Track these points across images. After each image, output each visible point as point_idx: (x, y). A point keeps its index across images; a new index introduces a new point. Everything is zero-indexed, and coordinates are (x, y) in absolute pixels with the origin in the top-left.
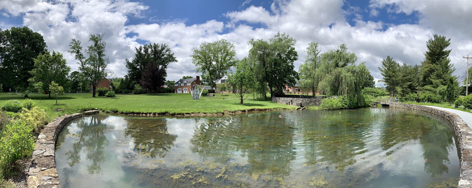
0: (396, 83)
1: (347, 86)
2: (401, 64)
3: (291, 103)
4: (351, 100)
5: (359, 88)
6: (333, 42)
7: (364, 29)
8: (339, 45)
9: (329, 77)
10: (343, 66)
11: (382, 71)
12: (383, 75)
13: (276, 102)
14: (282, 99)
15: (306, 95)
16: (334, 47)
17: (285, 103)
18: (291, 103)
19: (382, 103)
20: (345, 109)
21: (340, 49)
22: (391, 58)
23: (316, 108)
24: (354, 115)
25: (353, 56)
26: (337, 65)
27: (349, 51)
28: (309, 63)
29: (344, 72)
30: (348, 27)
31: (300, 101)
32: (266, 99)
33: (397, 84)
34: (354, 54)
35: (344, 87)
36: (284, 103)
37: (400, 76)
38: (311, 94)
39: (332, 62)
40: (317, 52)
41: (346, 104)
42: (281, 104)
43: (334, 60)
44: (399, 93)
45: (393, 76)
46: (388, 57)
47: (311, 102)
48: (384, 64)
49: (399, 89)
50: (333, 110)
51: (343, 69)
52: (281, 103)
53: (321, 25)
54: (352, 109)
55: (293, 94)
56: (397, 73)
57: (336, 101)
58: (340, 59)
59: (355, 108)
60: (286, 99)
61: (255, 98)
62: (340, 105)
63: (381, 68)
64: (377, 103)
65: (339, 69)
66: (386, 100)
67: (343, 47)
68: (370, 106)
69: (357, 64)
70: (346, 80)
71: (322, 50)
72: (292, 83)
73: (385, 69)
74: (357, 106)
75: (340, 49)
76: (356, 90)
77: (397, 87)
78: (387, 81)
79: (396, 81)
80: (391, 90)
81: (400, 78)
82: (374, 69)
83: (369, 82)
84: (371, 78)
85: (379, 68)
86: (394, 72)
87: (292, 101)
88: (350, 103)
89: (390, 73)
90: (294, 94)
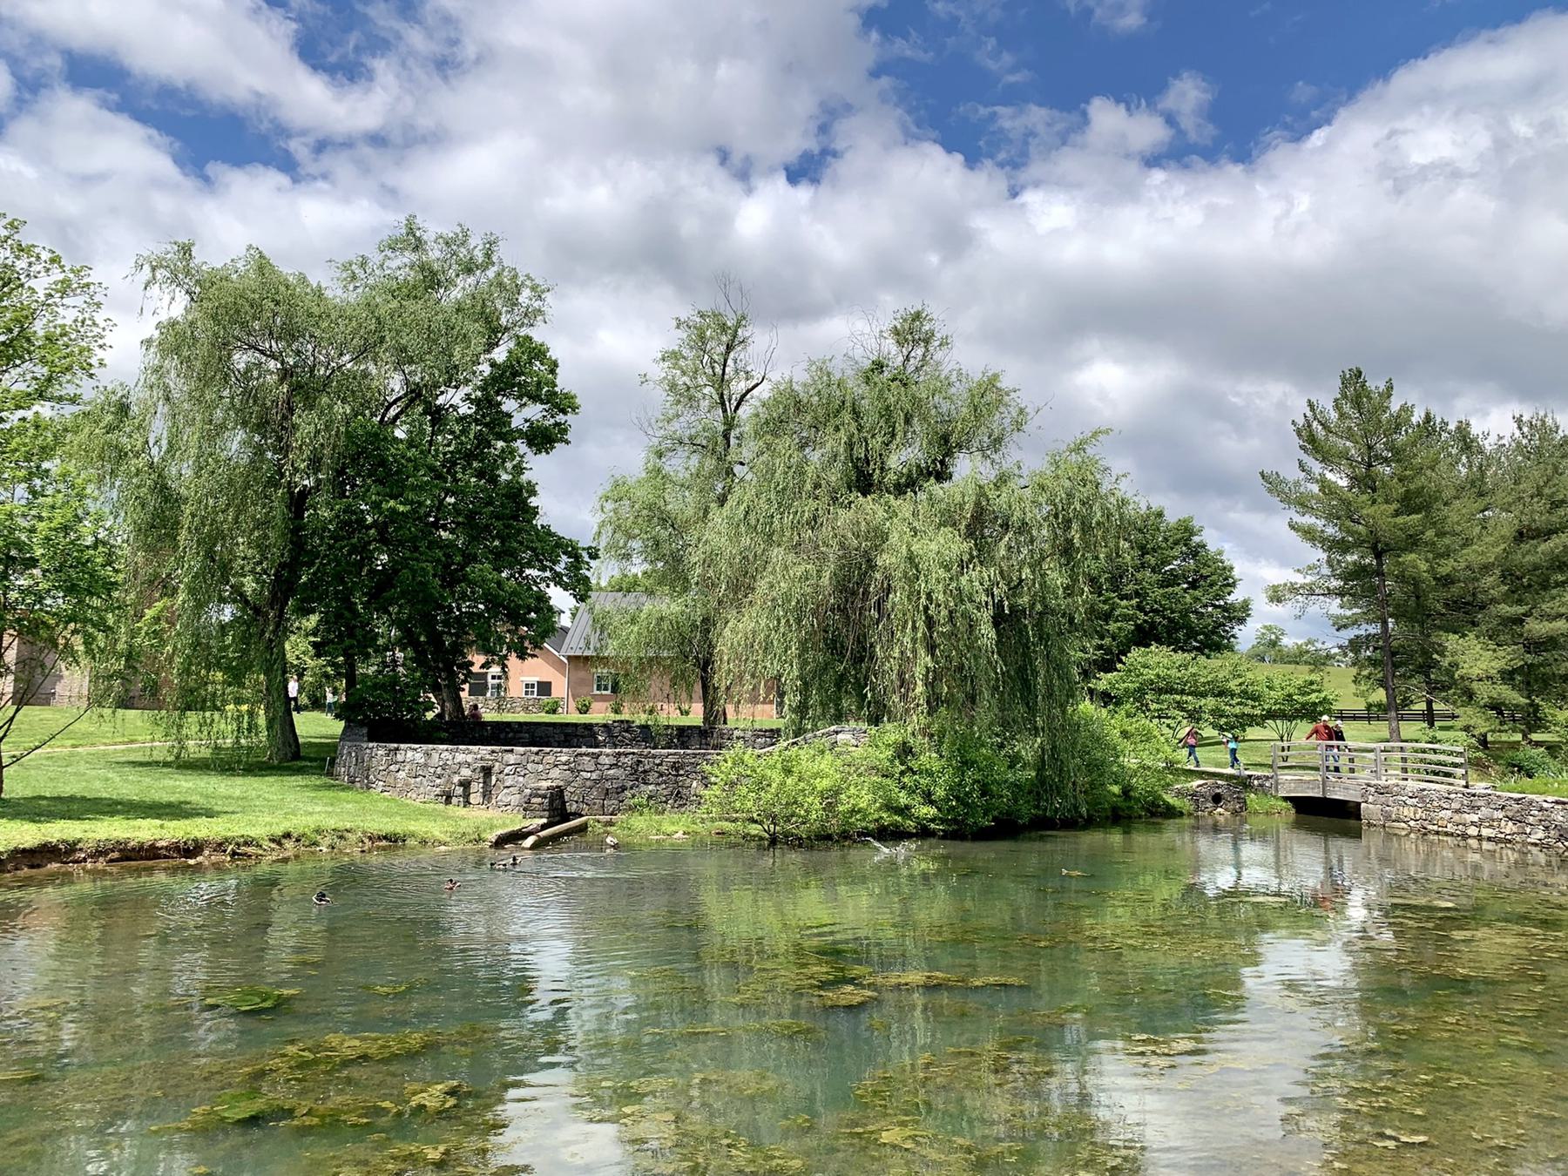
0: (1455, 605)
1: (931, 648)
2: (1496, 423)
3: (476, 787)
4: (966, 764)
5: (1058, 667)
6: (848, 294)
7: (1068, 162)
8: (888, 323)
9: (792, 576)
10: (907, 485)
11: (1303, 504)
12: (1309, 534)
13: (361, 780)
14: (412, 754)
15: (641, 718)
16: (852, 337)
17: (428, 789)
18: (476, 787)
19: (1296, 783)
20: (924, 833)
21: (892, 351)
22: (1375, 384)
23: (674, 827)
24: (1010, 885)
25: (987, 398)
26: (863, 481)
27: (964, 358)
28: (681, 465)
29: (918, 541)
30: (932, 173)
31: (551, 768)
32: (292, 758)
33: (1465, 611)
34: (992, 382)
35: (904, 656)
36: (423, 795)
37: (1483, 541)
38: (696, 717)
39: (823, 458)
40: (738, 387)
41: (928, 798)
42: (416, 803)
43: (834, 442)
44: (1484, 692)
45: (1412, 542)
46: (1353, 382)
47: (639, 775)
48: (1311, 443)
49: (1475, 657)
50: (828, 840)
51: (904, 506)
52: (407, 789)
53: (742, 171)
54: (983, 835)
55: (569, 715)
56: (1455, 514)
57: (845, 764)
58: (889, 431)
59: (1006, 829)
60: (442, 753)
61: (161, 749)
62: (862, 798)
63: (1292, 474)
64: (1245, 783)
65: (871, 508)
66: (1375, 763)
67: (912, 331)
68: (1171, 813)
69: (1027, 459)
70: (913, 595)
71: (775, 361)
72: (531, 625)
73: (1325, 485)
74: (1032, 811)
75: (892, 351)
76: (1020, 682)
77: (1451, 641)
78: (1359, 584)
79: (1446, 581)
80: (1405, 666)
81: (1488, 549)
82: (1222, 484)
83: (1176, 601)
84: (1211, 577)
85: (1272, 483)
86: (1411, 502)
87: (487, 771)
88: (954, 790)
89: (1381, 515)
90: (574, 717)
